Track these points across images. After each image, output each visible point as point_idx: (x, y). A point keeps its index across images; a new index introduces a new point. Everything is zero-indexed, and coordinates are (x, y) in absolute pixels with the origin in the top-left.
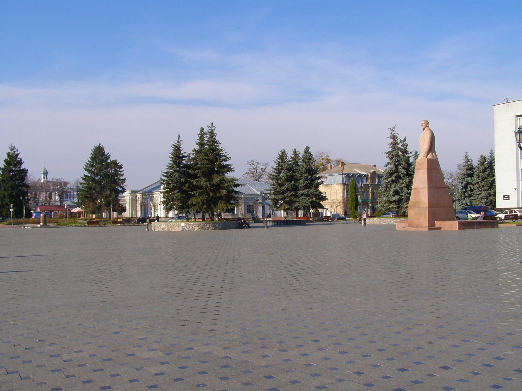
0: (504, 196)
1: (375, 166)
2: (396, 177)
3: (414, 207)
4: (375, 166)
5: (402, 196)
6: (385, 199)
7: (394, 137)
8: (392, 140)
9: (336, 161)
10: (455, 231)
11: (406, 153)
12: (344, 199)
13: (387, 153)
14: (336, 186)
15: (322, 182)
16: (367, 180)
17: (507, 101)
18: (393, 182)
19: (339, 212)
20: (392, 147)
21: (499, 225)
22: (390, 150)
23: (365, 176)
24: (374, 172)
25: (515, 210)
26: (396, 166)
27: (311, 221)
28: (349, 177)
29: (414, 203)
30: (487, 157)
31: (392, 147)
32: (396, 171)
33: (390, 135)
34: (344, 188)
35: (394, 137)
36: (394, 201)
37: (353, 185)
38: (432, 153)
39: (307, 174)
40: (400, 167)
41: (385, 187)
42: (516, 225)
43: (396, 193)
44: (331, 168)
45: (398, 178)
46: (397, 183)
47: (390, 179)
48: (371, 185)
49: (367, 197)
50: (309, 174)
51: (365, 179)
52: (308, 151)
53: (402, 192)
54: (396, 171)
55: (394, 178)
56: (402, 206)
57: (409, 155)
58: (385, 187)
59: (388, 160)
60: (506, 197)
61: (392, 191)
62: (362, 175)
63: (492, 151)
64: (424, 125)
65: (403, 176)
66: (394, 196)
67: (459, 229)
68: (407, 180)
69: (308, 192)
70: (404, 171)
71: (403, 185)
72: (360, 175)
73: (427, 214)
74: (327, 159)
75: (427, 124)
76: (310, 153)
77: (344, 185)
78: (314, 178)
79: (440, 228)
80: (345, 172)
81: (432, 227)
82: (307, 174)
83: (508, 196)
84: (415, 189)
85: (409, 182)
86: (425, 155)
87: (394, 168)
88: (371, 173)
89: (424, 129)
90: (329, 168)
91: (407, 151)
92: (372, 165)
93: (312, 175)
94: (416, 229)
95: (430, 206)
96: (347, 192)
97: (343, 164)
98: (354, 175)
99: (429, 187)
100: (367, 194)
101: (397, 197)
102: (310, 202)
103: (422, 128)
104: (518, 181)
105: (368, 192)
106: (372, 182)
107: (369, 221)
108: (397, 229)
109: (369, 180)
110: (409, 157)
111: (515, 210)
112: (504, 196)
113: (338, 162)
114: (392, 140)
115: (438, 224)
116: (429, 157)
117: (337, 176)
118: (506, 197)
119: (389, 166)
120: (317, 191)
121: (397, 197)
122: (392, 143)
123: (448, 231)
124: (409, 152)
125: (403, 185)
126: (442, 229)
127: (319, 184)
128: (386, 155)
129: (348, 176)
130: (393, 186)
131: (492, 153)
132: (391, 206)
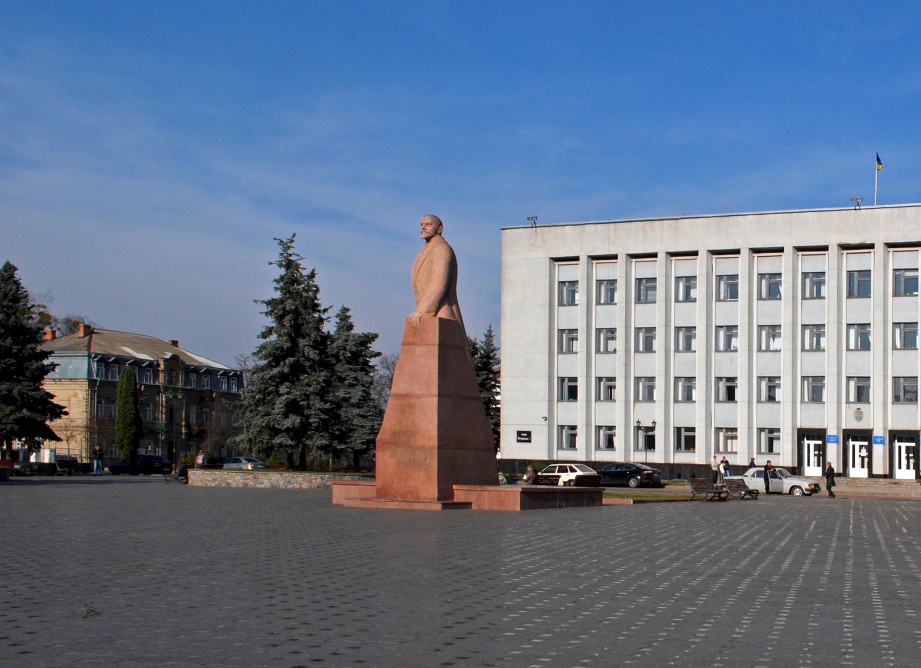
0: (519, 433)
1: (175, 343)
2: (292, 366)
3: (396, 444)
4: (175, 343)
5: (308, 417)
6: (259, 421)
7: (289, 265)
8: (283, 271)
9: (67, 321)
10: (516, 512)
11: (315, 311)
12: (91, 420)
13: (269, 303)
14: (71, 386)
15: (53, 366)
16: (156, 376)
17: (533, 223)
18: (283, 378)
19: (77, 453)
20: (282, 289)
21: (605, 501)
22: (278, 295)
23: (151, 364)
24: (175, 358)
25: (573, 466)
26: (293, 340)
27: (18, 473)
28: (107, 365)
29: (395, 434)
30: (479, 345)
31: (282, 289)
32: (293, 350)
33: (278, 258)
34: (93, 392)
35: (289, 265)
36: (288, 430)
37: (122, 385)
38: (451, 305)
39: (9, 341)
40: (302, 342)
41: (260, 391)
42: (635, 502)
43: (292, 407)
44: (54, 337)
45: (297, 370)
46: (293, 382)
47: (275, 371)
48: (166, 389)
49: (155, 419)
50: (15, 342)
51: (150, 374)
52: (12, 276)
53: (309, 407)
54: (293, 350)
55: (286, 370)
56: (309, 442)
57: (324, 316)
58: (260, 391)
59: (270, 322)
60: (524, 436)
61: (279, 406)
62: (143, 361)
63: (490, 331)
64: (429, 229)
65: (310, 367)
66: (286, 415)
67: (523, 506)
68: (323, 375)
69: (10, 391)
70: (313, 354)
71: (311, 389)
72: (137, 363)
73: (435, 465)
74: (41, 314)
75: (438, 227)
76: (17, 284)
77: (92, 383)
78: (27, 352)
79: (468, 505)
80: (95, 349)
81: (445, 495)
82: (9, 341)
83: (529, 434)
84: (398, 396)
85: (324, 381)
86: (433, 308)
87: (288, 345)
88: (166, 360)
89: (428, 240)
90: (48, 337)
91: (317, 305)
92: (167, 339)
93: (23, 344)
94: (404, 506)
95: (442, 446)
96: (99, 402)
97: (89, 331)
98: (120, 361)
99: (441, 395)
100: (155, 410)
101: (294, 420)
102: (16, 421)
103: (424, 235)
104: (550, 401)
105: (156, 404)
106: (170, 382)
107: (197, 477)
108: (334, 502)
109: (162, 375)
110: (321, 320)
111: (573, 466)
112: (519, 433)
113: (72, 325)
114: (283, 271)
115: (460, 493)
116: (444, 313)
117: (73, 360)
118: (524, 436)
119: (274, 337)
120: (37, 389)
121: (294, 420)
122: (282, 278)
123: (491, 513)
124: (322, 308)
125: (311, 389)
126: (474, 507)
127: (45, 371)
128: (265, 308)
129: (103, 360)
130: (283, 389)
131: (489, 336)
132: (277, 440)
